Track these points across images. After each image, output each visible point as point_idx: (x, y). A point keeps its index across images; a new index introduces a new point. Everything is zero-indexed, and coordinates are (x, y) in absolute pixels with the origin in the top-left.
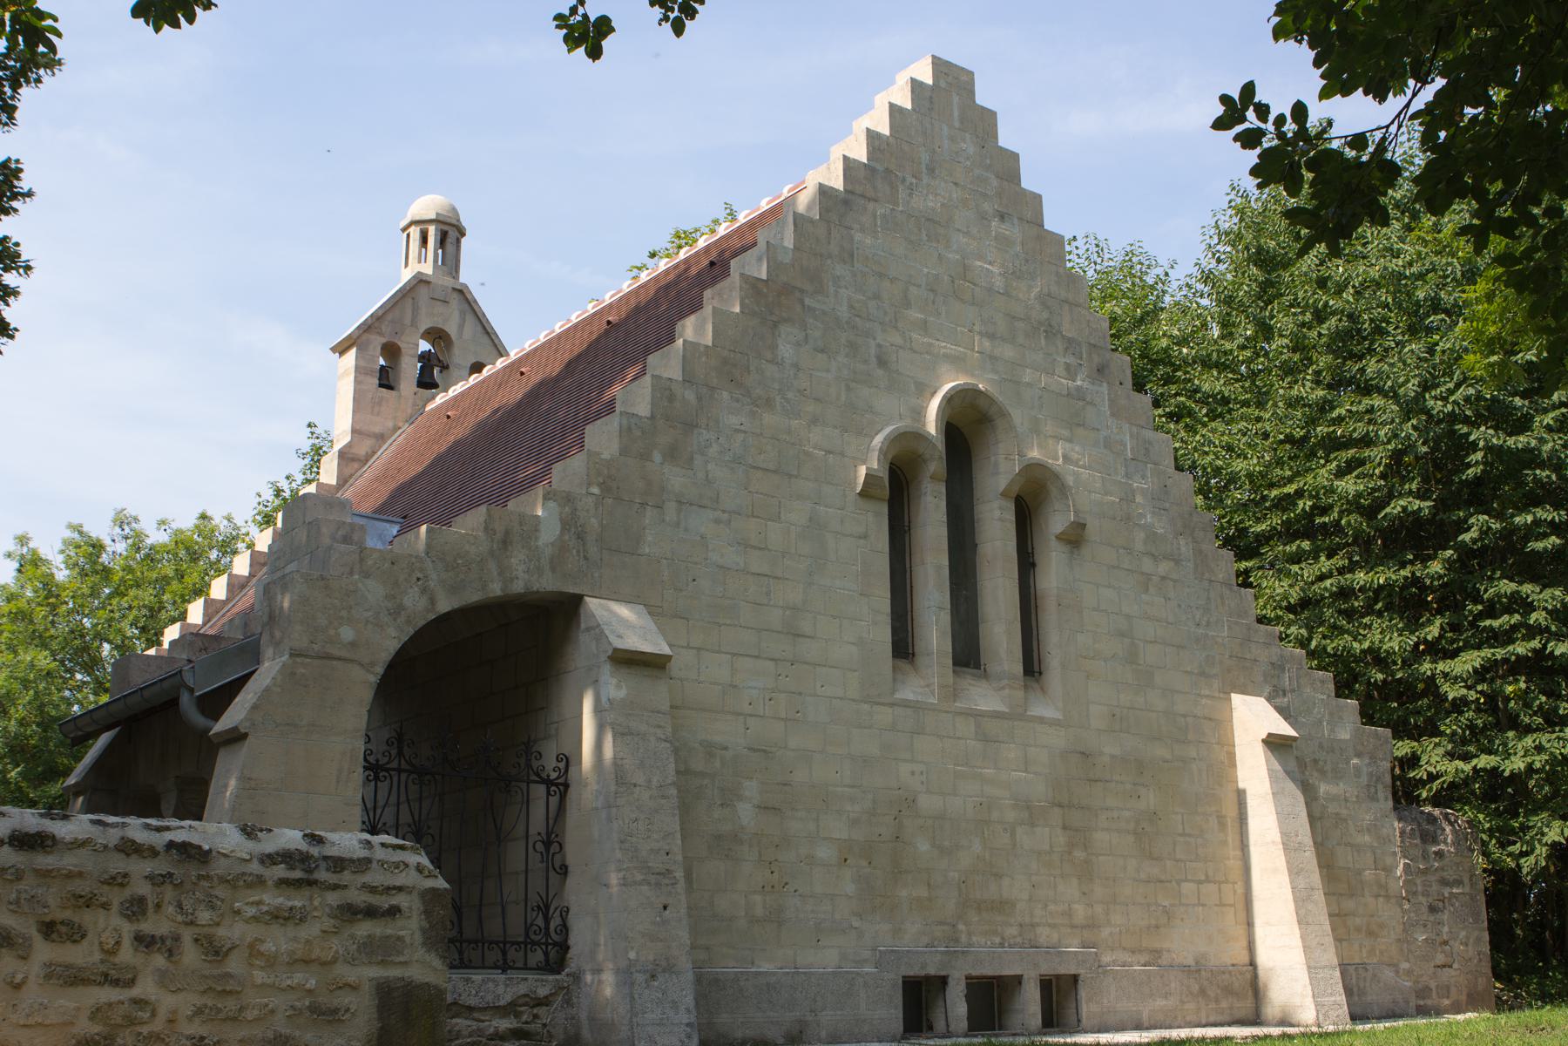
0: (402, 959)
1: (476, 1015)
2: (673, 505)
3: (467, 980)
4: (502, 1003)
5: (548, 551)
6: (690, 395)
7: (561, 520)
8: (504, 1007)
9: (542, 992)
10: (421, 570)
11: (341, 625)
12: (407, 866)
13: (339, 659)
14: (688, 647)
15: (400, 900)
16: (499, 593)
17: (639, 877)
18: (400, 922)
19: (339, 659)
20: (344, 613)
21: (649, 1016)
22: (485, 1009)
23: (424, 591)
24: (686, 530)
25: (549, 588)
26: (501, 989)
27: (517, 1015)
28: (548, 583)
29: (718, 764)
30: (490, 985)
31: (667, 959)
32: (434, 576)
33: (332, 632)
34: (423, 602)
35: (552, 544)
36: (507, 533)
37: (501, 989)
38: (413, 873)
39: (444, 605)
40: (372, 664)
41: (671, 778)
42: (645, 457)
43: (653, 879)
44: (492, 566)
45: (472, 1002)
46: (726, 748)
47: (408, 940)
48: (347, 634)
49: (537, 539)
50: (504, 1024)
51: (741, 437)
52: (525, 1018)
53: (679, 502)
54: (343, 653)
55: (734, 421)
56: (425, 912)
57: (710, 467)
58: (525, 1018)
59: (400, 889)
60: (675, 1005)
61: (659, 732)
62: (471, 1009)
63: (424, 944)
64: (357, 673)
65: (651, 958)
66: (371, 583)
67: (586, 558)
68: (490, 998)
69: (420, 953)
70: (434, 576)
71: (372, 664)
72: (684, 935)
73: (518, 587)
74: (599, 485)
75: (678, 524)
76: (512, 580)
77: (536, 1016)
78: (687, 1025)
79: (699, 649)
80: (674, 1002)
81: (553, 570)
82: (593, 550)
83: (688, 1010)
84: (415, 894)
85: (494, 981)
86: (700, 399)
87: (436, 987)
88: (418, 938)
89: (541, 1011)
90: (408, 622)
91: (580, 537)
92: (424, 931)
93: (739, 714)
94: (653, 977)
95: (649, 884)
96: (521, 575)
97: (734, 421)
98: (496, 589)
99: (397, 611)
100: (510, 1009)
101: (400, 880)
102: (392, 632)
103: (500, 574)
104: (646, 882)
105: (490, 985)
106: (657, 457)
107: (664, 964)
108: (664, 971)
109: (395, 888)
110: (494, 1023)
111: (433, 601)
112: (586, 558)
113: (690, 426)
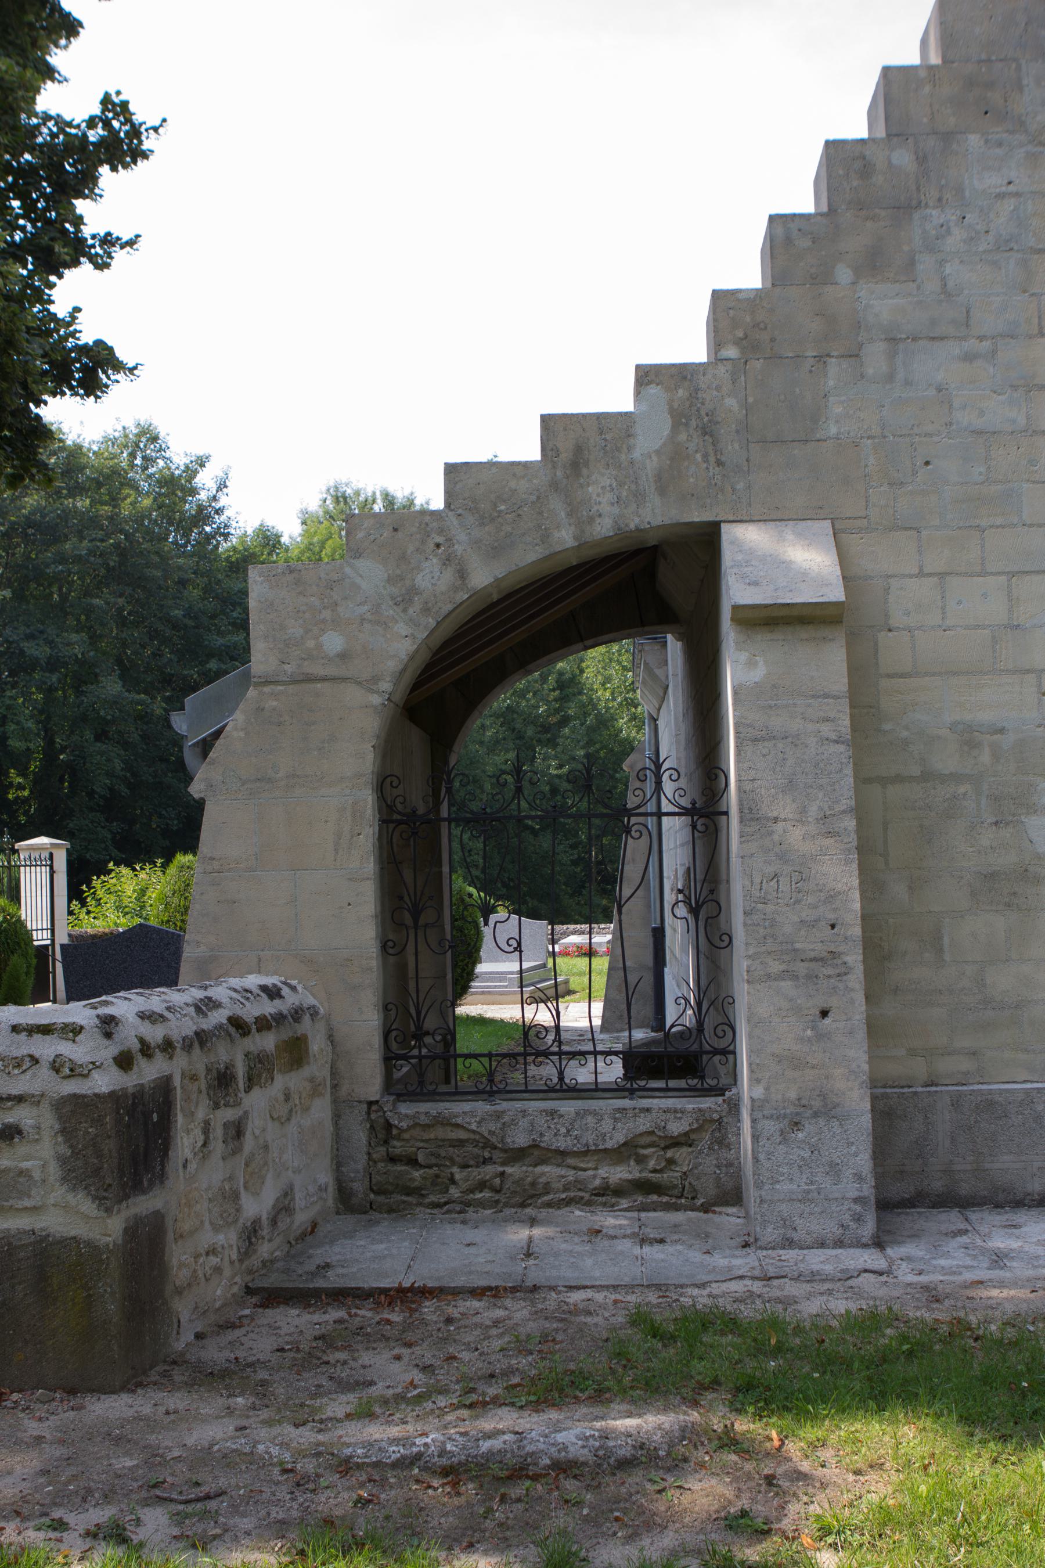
0: (27, 1203)
1: (571, 1161)
2: (881, 346)
3: (552, 1113)
4: (609, 1144)
5: (652, 465)
6: (903, 158)
7: (672, 411)
8: (613, 1150)
9: (676, 1128)
10: (441, 531)
11: (323, 631)
12: (35, 1060)
13: (324, 679)
14: (921, 574)
15: (22, 1116)
16: (570, 543)
17: (776, 967)
18: (21, 1148)
19: (324, 679)
20: (327, 614)
21: (784, 1187)
22: (586, 1153)
23: (447, 561)
24: (908, 383)
25: (657, 521)
26: (607, 1125)
27: (641, 1160)
28: (655, 515)
29: (986, 757)
30: (590, 1120)
31: (823, 1096)
32: (462, 537)
33: (311, 644)
34: (448, 577)
35: (658, 452)
36: (579, 449)
37: (607, 1125)
38: (44, 1072)
39: (484, 576)
40: (375, 679)
41: (846, 799)
42: (822, 277)
43: (802, 968)
44: (557, 505)
45: (561, 1144)
46: (1001, 731)
47: (37, 1175)
48: (333, 642)
49: (630, 449)
50: (619, 1173)
51: (1009, 205)
52: (652, 1164)
53: (892, 340)
54: (331, 671)
55: (993, 181)
56: (63, 1131)
57: (948, 269)
58: (652, 1164)
59: (20, 1099)
60: (834, 1169)
61: (826, 730)
62: (563, 1154)
63: (64, 1179)
64: (354, 695)
65: (793, 1095)
66: (364, 565)
67: (719, 463)
68: (589, 1138)
69: (59, 1193)
70: (462, 537)
71: (375, 679)
72: (858, 1054)
73: (603, 528)
74: (737, 342)
75: (890, 377)
76: (591, 520)
77: (671, 1162)
78: (856, 1200)
79: (942, 575)
80: (832, 1165)
81: (662, 491)
82: (732, 449)
83: (859, 1177)
84: (45, 1105)
85: (594, 1113)
86: (921, 159)
87: (89, 1243)
88: (54, 1170)
89: (680, 1153)
90: (426, 610)
91: (708, 431)
92: (62, 1161)
93: (1028, 671)
94: (796, 1125)
95: (795, 977)
96: (605, 508)
97: (993, 181)
98: (565, 538)
99: (404, 601)
100: (627, 1151)
101: (20, 1085)
102: (402, 628)
103: (569, 515)
104: (787, 974)
105: (590, 1120)
106: (844, 274)
107: (817, 1104)
108: (816, 1115)
109: (10, 1098)
110: (602, 1172)
111: (462, 574)
112: (719, 463)
113: (905, 208)
